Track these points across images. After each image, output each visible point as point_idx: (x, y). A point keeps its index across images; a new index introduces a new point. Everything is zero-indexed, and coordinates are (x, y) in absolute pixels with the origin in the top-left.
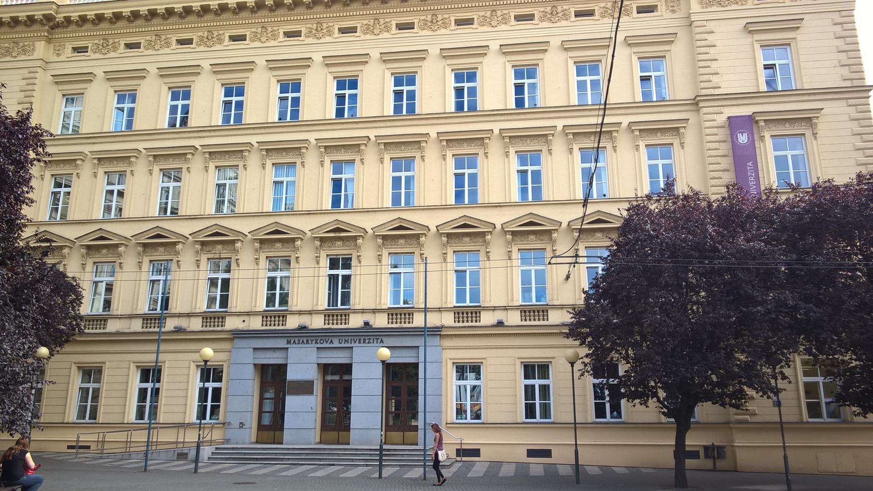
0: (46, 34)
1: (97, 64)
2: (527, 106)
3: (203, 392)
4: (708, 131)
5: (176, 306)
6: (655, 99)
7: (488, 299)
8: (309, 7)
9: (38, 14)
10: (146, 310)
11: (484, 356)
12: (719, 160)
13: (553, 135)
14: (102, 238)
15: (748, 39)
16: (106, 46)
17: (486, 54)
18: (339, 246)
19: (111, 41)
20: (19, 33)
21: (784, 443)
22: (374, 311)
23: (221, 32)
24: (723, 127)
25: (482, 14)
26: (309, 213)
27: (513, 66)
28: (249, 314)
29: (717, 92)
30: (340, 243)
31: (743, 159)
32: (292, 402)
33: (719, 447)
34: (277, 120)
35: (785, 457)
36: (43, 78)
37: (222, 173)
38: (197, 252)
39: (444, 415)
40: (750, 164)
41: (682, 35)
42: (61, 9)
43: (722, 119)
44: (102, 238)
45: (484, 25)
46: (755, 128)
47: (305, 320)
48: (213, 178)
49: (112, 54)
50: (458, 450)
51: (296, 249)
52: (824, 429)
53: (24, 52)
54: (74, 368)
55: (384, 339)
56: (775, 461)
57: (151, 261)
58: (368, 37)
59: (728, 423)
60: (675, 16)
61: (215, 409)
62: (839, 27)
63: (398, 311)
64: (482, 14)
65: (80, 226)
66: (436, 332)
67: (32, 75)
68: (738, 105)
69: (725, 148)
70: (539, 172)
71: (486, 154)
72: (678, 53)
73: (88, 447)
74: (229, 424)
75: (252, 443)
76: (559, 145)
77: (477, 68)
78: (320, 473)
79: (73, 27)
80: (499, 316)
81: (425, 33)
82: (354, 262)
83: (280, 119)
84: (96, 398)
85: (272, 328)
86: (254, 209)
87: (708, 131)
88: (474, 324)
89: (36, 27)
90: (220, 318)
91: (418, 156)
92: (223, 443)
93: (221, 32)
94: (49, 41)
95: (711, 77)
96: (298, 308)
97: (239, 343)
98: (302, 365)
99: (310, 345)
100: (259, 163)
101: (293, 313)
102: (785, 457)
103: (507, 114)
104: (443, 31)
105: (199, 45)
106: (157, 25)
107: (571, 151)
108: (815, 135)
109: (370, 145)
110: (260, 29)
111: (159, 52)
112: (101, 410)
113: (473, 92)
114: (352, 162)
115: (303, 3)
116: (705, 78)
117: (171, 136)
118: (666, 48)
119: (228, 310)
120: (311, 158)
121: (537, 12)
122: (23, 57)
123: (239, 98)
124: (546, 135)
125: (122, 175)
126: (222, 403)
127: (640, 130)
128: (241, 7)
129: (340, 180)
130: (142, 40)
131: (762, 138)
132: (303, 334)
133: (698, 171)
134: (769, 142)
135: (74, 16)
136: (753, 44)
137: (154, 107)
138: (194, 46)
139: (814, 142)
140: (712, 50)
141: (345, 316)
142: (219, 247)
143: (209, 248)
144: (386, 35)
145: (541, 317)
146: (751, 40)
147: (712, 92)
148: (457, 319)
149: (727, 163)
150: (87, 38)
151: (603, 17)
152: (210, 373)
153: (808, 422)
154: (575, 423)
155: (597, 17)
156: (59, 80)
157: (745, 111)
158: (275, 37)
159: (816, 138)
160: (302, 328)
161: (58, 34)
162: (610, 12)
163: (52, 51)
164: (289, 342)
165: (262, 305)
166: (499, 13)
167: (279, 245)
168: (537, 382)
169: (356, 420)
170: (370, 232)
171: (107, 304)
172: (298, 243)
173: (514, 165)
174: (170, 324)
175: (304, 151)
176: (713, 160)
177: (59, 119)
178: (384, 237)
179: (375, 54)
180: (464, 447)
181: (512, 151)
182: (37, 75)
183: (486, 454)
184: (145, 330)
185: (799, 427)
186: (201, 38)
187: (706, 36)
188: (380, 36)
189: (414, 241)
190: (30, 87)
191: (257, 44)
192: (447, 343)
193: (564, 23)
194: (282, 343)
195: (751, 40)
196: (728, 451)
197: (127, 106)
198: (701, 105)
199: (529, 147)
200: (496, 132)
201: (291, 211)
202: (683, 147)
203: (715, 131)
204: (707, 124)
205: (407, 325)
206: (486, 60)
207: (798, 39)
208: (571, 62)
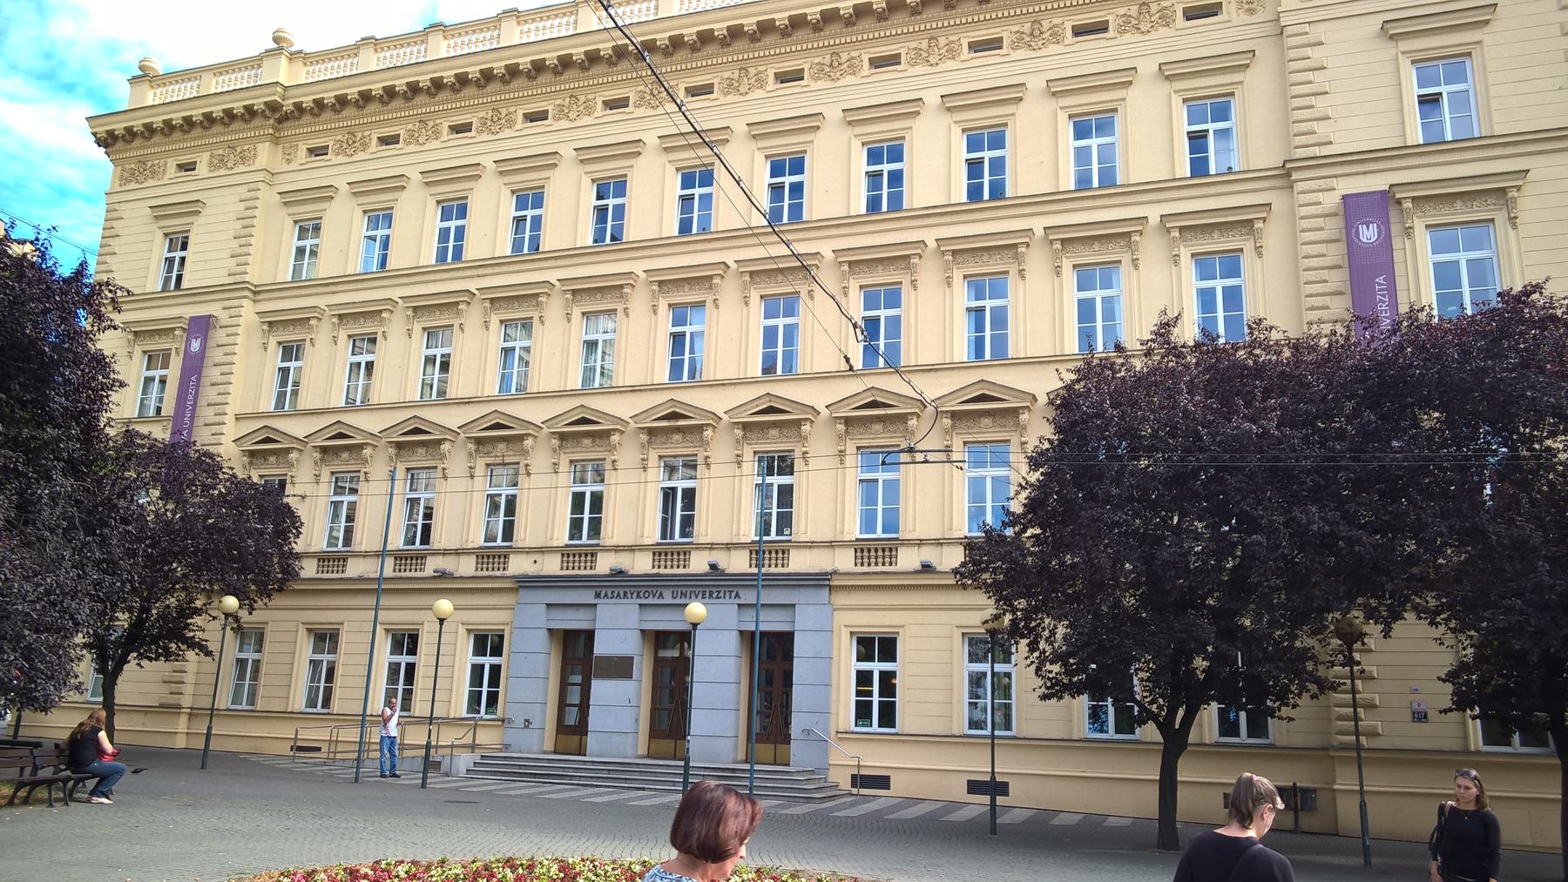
1: (339, 172)
2: (1212, 171)
3: (477, 671)
4: (1305, 224)
5: (440, 539)
6: (1096, 184)
7: (802, 528)
8: (915, 11)
9: (258, 103)
10: (481, 542)
12: (1325, 274)
13: (1141, 233)
14: (268, 440)
15: (1389, 50)
16: (495, 123)
17: (1021, 99)
18: (876, 433)
19: (359, 135)
20: (237, 132)
21: (1361, 785)
22: (729, 547)
23: (854, 54)
24: (1336, 215)
25: (913, 45)
26: (633, 390)
27: (1070, 117)
28: (542, 550)
29: (1326, 151)
30: (677, 437)
31: (1368, 269)
32: (601, 689)
33: (1305, 791)
34: (590, 243)
36: (268, 197)
37: (592, 324)
38: (470, 455)
39: (833, 717)
40: (1380, 280)
41: (1265, 52)
42: (290, 93)
43: (1332, 200)
45: (916, 64)
46: (1393, 216)
47: (623, 561)
48: (579, 331)
49: (361, 156)
50: (854, 777)
51: (612, 448)
52: (871, 738)
53: (154, 174)
54: (302, 631)
55: (742, 592)
57: (408, 470)
58: (731, 99)
59: (1327, 749)
60: (1254, 19)
61: (493, 699)
63: (880, 545)
64: (913, 45)
65: (314, 418)
66: (820, 581)
67: (252, 194)
68: (1365, 173)
69: (1336, 253)
70: (897, 319)
71: (1021, 273)
73: (319, 749)
74: (510, 721)
75: (643, 757)
77: (1232, 94)
79: (307, 118)
80: (929, 555)
81: (821, 84)
82: (798, 465)
83: (595, 241)
84: (331, 672)
85: (576, 572)
86: (732, 373)
87: (1305, 224)
88: (887, 568)
89: (257, 122)
90: (503, 556)
91: (1013, 270)
92: (500, 750)
94: (276, 141)
95: (1315, 126)
96: (615, 541)
97: (526, 595)
98: (618, 630)
99: (727, 600)
100: (562, 313)
101: (606, 549)
102: (1363, 806)
104: (849, 80)
105: (480, 132)
106: (421, 106)
107: (1058, 271)
108: (1513, 220)
109: (730, 275)
111: (1040, 53)
112: (337, 694)
113: (998, 165)
114: (702, 304)
115: (905, 6)
116: (1303, 127)
117: (438, 276)
118: (808, 137)
119: (601, 542)
120: (639, 301)
121: (1111, 16)
122: (242, 168)
123: (895, 166)
124: (1015, 246)
125: (527, 325)
126: (501, 690)
127: (1181, 229)
128: (861, 12)
129: (683, 335)
131: (1408, 232)
132: (619, 582)
133: (1287, 297)
134: (1423, 239)
135: (307, 101)
136: (1397, 59)
137: (416, 232)
138: (472, 134)
139: (1512, 233)
140: (1318, 77)
141: (684, 553)
142: (502, 446)
143: (488, 448)
144: (758, 93)
146: (1394, 51)
147: (1317, 151)
149: (1338, 279)
150: (327, 132)
151: (1122, 33)
152: (878, 646)
153: (1478, 753)
154: (364, 715)
155: (1111, 33)
156: (290, 199)
157: (1377, 183)
158: (589, 111)
159: (1515, 227)
160: (619, 573)
161: (289, 129)
162: (1134, 22)
163: (280, 155)
164: (598, 596)
165: (562, 537)
166: (942, 41)
167: (587, 442)
168: (876, 667)
169: (701, 722)
170: (825, 412)
171: (348, 540)
172: (615, 438)
173: (962, 298)
174: (432, 565)
175: (915, 260)
176: (1312, 275)
177: (289, 257)
178: (746, 427)
179: (932, 98)
180: (864, 772)
181: (957, 275)
182: (259, 194)
183: (899, 786)
184: (398, 574)
185: (230, 714)
186: (483, 121)
187: (1308, 51)
188: (750, 96)
189: (793, 432)
190: (249, 213)
191: (564, 124)
192: (841, 599)
193: (1053, 49)
194: (587, 597)
195: (1394, 51)
196: (1322, 801)
197: (380, 233)
198: (1295, 176)
199: (986, 266)
200: (1039, 232)
201: (524, 394)
202: (1260, 255)
203: (1320, 222)
204: (1304, 211)
205: (780, 570)
206: (918, 124)
207: (1485, 43)
208: (1063, 117)
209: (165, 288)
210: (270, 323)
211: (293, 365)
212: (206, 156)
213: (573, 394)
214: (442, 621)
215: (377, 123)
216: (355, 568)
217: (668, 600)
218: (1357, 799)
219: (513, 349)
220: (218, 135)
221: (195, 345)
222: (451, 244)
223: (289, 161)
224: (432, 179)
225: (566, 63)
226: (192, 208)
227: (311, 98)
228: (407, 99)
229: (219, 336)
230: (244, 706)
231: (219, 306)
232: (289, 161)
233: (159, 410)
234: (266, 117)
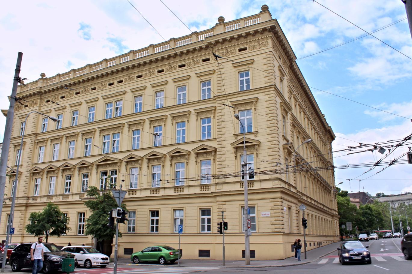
0: (271, 35)
6: (245, 90)
11: (68, 211)
35: (224, 247)
42: (42, 89)
44: (204, 149)
52: (206, 235)
53: (264, 46)
72: (214, 79)
78: (314, 261)
102: (224, 247)
103: (175, 107)
105: (30, 107)
110: (256, 43)
130: (80, 91)
135: (76, 81)
145: (251, 186)
148: (151, 193)
152: (155, 213)
168: (206, 217)
186: (146, 75)
210: (198, 113)
213: (200, 141)
215: (92, 85)
218: (222, 246)
219: (115, 141)
222: (245, 85)
225: (169, 57)
230: (206, 231)
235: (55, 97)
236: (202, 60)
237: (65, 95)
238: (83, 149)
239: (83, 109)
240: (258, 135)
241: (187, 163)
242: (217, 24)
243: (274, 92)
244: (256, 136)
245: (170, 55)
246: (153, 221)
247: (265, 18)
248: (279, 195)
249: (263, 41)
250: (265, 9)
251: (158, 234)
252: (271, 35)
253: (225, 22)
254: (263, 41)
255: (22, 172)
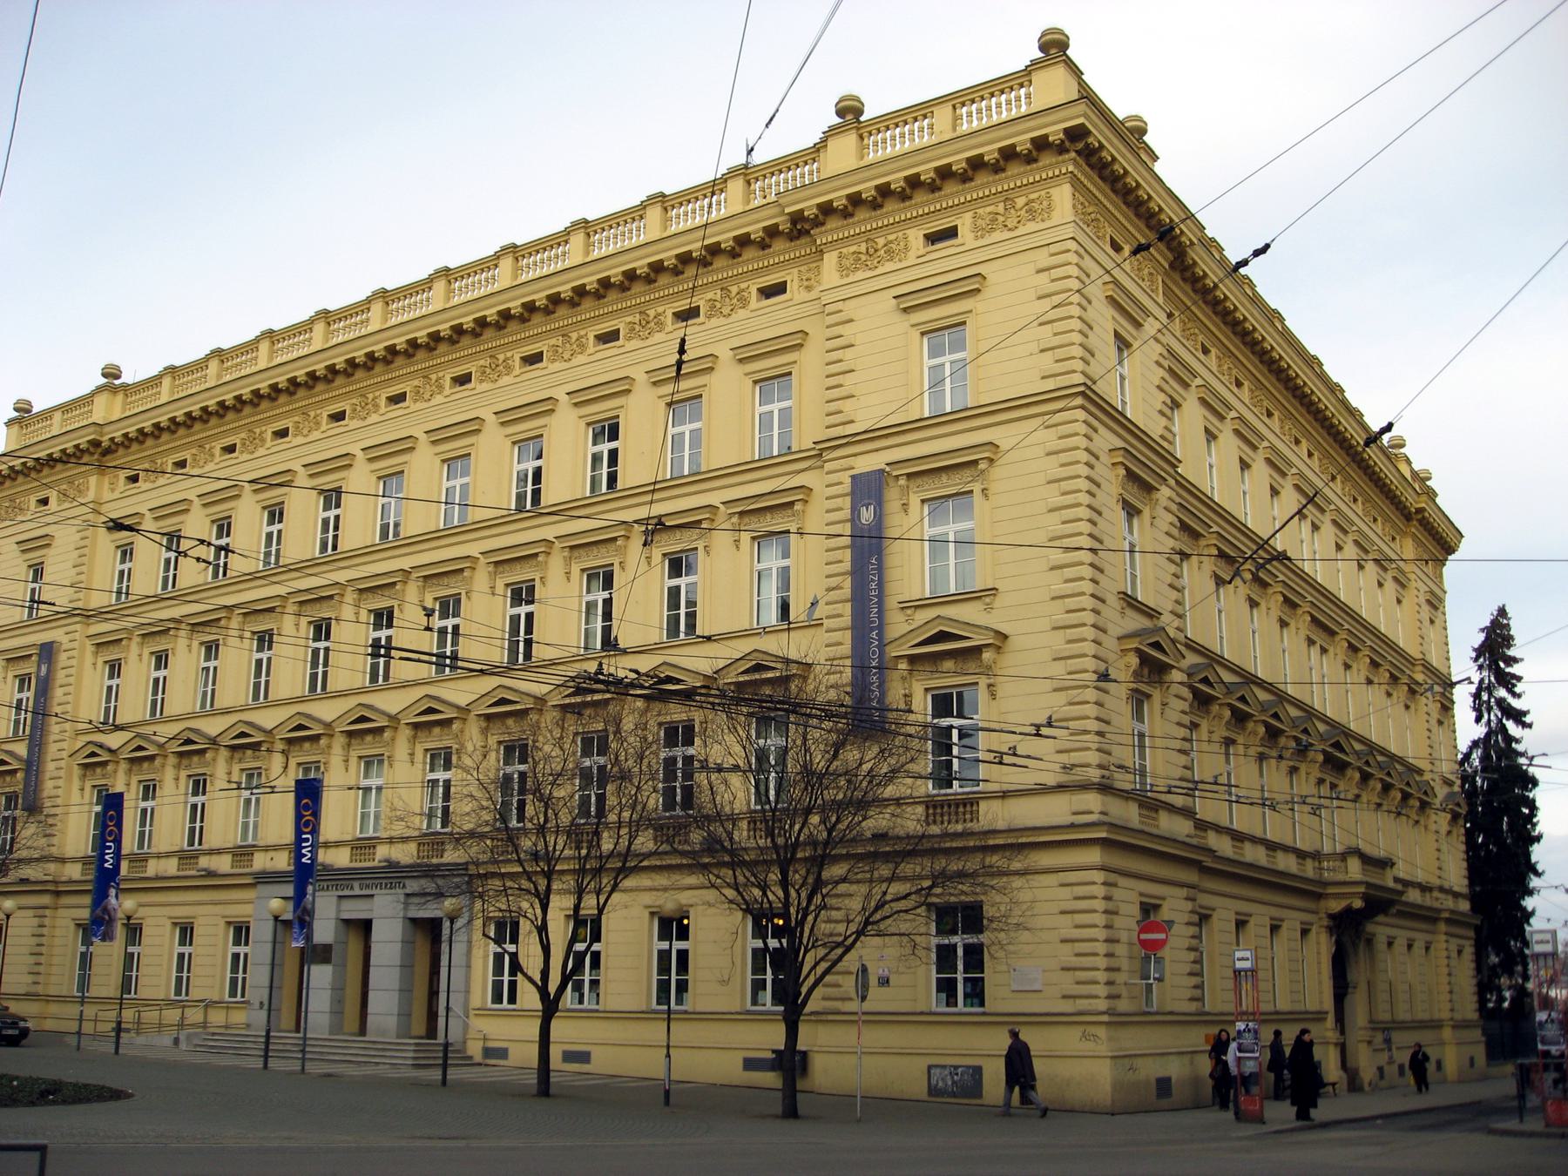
0: (1071, 168)
16: (496, 369)
23: (743, 286)
29: (850, 429)
53: (1032, 214)
55: (407, 882)
56: (649, 1064)
62: (1044, 276)
68: (877, 450)
72: (809, 366)
76: (556, 562)
93: (743, 286)
111: (648, 342)
130: (620, 324)
138: (702, 318)
180: (491, 1044)
209: (520, 508)
211: (682, 582)
212: (968, 217)
214: (8, 917)
215: (219, 434)
216: (153, 868)
217: (357, 891)
220: (985, 183)
221: (867, 515)
223: (113, 490)
224: (582, 398)
226: (45, 542)
227: (362, 352)
228: (292, 394)
229: (63, 659)
230: (239, 998)
231: (61, 631)
232: (113, 490)
233: (785, 608)
234: (92, 454)
235: (363, 396)
236: (523, 359)
237: (408, 390)
238: (192, 685)
239: (424, 469)
240: (999, 602)
241: (989, 686)
242: (1034, 63)
243: (1081, 415)
244: (989, 608)
245: (831, 202)
246: (664, 956)
247: (1052, 88)
248: (1094, 856)
249: (891, 237)
250: (1054, 46)
251: (686, 1012)
252: (1071, 168)
253: (35, 410)
254: (891, 237)
255: (1006, 637)
